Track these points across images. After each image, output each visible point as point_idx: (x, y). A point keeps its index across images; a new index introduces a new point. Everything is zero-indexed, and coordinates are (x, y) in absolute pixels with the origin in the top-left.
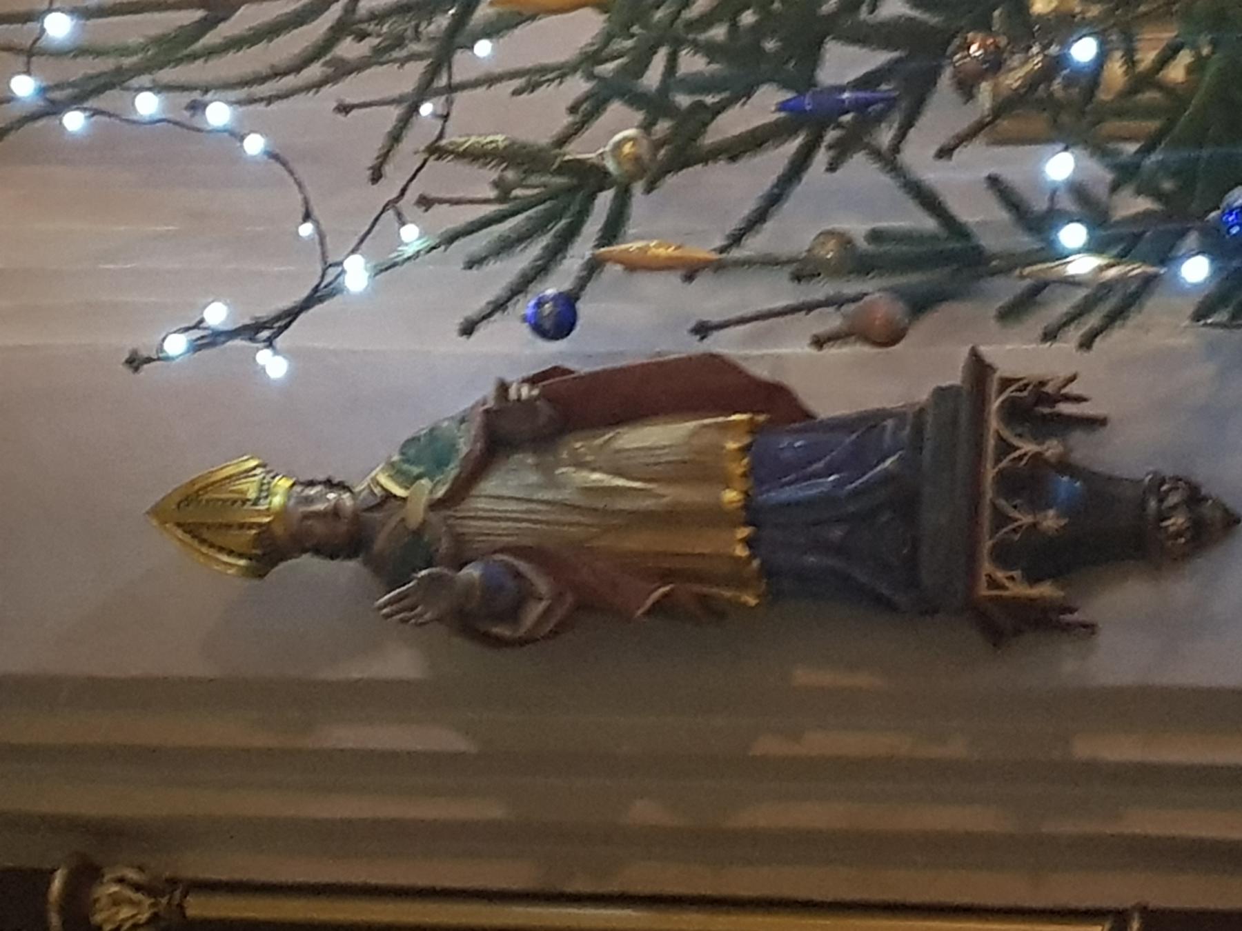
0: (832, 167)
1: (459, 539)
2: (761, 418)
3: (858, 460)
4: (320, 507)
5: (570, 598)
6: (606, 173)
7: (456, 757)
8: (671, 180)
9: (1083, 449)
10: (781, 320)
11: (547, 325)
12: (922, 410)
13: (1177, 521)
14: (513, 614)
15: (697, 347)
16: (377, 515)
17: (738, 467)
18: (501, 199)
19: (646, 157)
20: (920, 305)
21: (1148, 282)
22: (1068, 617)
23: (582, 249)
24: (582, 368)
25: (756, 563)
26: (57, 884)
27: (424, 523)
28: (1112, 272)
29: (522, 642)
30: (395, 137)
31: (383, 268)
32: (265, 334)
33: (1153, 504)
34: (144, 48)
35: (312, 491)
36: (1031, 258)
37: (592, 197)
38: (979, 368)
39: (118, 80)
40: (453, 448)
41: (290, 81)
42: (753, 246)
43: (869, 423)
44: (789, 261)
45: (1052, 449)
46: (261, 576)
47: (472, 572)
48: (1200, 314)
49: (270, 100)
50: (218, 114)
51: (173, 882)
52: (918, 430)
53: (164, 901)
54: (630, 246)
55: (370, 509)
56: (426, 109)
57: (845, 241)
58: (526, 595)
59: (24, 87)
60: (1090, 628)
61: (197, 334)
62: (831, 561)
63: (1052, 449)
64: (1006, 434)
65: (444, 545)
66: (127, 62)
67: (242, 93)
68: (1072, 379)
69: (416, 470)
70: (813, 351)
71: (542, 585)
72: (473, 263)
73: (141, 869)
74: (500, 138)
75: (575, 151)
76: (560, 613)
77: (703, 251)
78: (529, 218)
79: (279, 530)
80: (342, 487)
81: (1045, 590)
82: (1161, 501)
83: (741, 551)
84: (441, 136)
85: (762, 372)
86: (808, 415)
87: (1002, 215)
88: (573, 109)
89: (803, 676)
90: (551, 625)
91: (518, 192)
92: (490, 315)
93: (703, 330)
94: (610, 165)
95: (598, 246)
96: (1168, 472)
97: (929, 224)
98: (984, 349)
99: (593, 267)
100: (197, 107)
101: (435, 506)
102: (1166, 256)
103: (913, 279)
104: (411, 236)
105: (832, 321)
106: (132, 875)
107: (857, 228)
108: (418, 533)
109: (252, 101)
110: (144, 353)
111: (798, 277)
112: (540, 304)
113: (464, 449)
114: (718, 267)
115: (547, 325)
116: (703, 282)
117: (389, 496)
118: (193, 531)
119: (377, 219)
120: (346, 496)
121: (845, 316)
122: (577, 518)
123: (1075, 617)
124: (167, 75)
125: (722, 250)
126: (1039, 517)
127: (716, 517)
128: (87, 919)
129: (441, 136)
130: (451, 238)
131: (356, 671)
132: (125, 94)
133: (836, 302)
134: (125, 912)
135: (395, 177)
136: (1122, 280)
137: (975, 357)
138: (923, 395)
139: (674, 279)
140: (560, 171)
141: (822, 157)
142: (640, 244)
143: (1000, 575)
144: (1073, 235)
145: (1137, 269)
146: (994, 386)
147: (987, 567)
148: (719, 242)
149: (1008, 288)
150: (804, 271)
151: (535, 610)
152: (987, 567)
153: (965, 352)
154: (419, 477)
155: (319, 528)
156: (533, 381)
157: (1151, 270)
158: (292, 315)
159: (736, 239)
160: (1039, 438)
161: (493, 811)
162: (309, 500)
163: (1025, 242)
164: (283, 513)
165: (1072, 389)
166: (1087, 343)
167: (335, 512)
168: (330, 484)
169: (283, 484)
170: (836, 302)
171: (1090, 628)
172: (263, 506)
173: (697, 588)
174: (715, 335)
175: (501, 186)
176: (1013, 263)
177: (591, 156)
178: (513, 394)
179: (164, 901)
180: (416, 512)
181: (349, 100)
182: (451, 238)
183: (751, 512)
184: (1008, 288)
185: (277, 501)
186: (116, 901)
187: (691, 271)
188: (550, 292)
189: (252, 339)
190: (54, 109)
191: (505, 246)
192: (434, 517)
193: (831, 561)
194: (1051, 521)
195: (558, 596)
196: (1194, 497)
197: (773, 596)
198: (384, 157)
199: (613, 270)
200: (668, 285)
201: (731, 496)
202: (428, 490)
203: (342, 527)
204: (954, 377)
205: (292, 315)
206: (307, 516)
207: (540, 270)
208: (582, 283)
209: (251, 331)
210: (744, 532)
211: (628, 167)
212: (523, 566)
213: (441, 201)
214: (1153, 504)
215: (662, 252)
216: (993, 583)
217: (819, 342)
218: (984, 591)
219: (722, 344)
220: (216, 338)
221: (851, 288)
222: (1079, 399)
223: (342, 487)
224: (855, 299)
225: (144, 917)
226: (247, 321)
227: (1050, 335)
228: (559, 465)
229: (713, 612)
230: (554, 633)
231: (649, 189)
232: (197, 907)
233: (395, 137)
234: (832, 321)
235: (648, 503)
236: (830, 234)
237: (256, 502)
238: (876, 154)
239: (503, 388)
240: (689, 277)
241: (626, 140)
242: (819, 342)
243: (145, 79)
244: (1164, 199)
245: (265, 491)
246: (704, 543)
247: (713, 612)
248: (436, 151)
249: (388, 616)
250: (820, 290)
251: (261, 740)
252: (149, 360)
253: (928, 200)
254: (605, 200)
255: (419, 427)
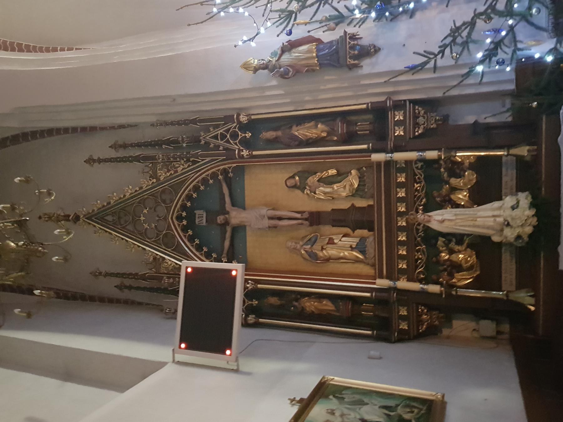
0: (323, 7)
1: (280, 65)
2: (317, 43)
3: (330, 47)
4: (262, 63)
5: (295, 72)
6: (294, 11)
7: (282, 94)
8: (302, 11)
9: (361, 42)
10: (319, 29)
11: (288, 34)
12: (338, 40)
13: (372, 50)
14: (288, 74)
15: (308, 34)
16: (269, 63)
17: (315, 50)
18: (280, 17)
19: (299, 8)
20: (337, 24)
21: (367, 17)
22: (359, 65)
23: (292, 23)
24: (293, 40)
25: (318, 63)
26: (237, 152)
27: (275, 64)
28: (363, 16)
29: (289, 78)
30: (265, 10)
31: (266, 29)
32: (251, 40)
33: (369, 48)
34: (229, 2)
35: (260, 61)
36: (351, 16)
37: (292, 14)
38: (345, 32)
39: (227, 7)
40: (278, 53)
41: (250, 4)
42: (314, 20)
43: (331, 42)
44: (319, 21)
45: (356, 42)
46: (255, 73)
47: (282, 69)
48: (374, 21)
49: (247, 7)
50: (241, 10)
51: (249, 114)
52: (338, 43)
53: (249, 117)
54: (298, 21)
55: (268, 63)
56: (269, 5)
57: (326, 17)
58: (289, 71)
59: (215, 10)
60: (362, 66)
61: (242, 41)
62: (328, 62)
63: (356, 42)
64: (349, 41)
65: (278, 66)
66: (228, 4)
67: (243, 7)
68: (358, 32)
69: (273, 56)
70: (323, 33)
71: (291, 70)
72: (277, 26)
73: (245, 113)
74: (279, 8)
75: (289, 9)
76: (294, 74)
77: (308, 21)
78: (284, 19)
79: (257, 67)
80: (264, 60)
81: (356, 62)
82: (370, 48)
83: (316, 62)
84: (271, 9)
85: (317, 37)
86: (323, 42)
87: (346, 10)
88: (287, 3)
89: (327, 78)
90: (293, 75)
91: (281, 16)
92: (280, 33)
93: (309, 32)
94: (294, 10)
95: (294, 22)
96: (371, 43)
97: (337, 13)
98: (346, 30)
99: (293, 25)
100: (238, 9)
101: (276, 61)
102: (370, 13)
103: (336, 21)
104: (269, 24)
105: (325, 28)
106: (244, 114)
107: (327, 15)
108: (274, 65)
109: (245, 8)
110: (237, 45)
111: (320, 23)
112: (287, 31)
113: (279, 53)
114: (309, 23)
115: (288, 34)
116: (308, 25)
117: (270, 60)
118: (246, 68)
119: (264, 22)
120: (265, 61)
121: (328, 28)
122: (294, 60)
123: (360, 65)
124: (234, 5)
125: (310, 20)
126: (355, 52)
127: (313, 58)
128: (239, 120)
129: (271, 9)
130: (274, 24)
131: (268, 84)
132: (228, 9)
133: (326, 25)
134: (244, 119)
135: (266, 15)
136: (364, 17)
137: (345, 31)
138: (338, 37)
139: (304, 25)
140: (288, 12)
141: (322, 5)
142: (299, 21)
143: (350, 60)
144: (357, 12)
145: (366, 15)
146: (347, 35)
147: (348, 60)
148: (309, 19)
149: (348, 21)
150: (321, 22)
151: (291, 73)
152: (348, 60)
153: (343, 31)
154: (273, 57)
155: (262, 66)
156: (287, 42)
157: (368, 15)
158: (255, 37)
159: (311, 19)
160: (354, 41)
161: (288, 100)
162: (260, 62)
163: (349, 14)
164: (257, 65)
165: (358, 34)
166: (359, 27)
167: (264, 63)
168: (262, 60)
169: (256, 61)
170: (326, 25)
171: (362, 66)
172: (254, 64)
173: (311, 68)
174: (311, 32)
175: (280, 15)
176: (348, 17)
177: (291, 9)
178: (285, 44)
179: (249, 117)
180: (274, 62)
181: (257, 6)
182: (274, 24)
183: (317, 56)
184: (348, 21)
185: (256, 63)
186: (243, 118)
187: (306, 24)
188: (288, 29)
189: (250, 41)
190: (219, 12)
191: (281, 24)
192: (276, 63)
193: (328, 62)
194: (356, 52)
195: (293, 71)
196: (375, 46)
197: (320, 68)
198: (264, 13)
199: (296, 25)
200: (303, 27)
201: (314, 55)
202: (275, 59)
203: (265, 65)
204: (342, 34)
205: (255, 37)
206: (260, 65)
207: (287, 26)
208: (292, 27)
209: (249, 40)
210: (317, 59)
211: (297, 10)
212: (289, 68)
213: (271, 19)
214: (369, 48)
215: (302, 21)
216: (349, 62)
217: (324, 32)
218: (348, 63)
219: (312, 34)
220: (245, 41)
221: (328, 23)
222: (359, 35)
223: (264, 60)
224: (329, 25)
225: (246, 119)
226: (249, 39)
227: (355, 26)
228: (291, 53)
229: (314, 71)
230: (293, 76)
231: (299, 13)
232: (253, 117)
233: (265, 10)
234: (325, 28)
235: (303, 57)
236: (324, 16)
237: (253, 64)
238: (329, 4)
239: (283, 44)
240: (306, 25)
241: (296, 6)
242: (324, 32)
243: (230, 6)
244: (126, 126)
245: (254, 62)
246: (311, 62)
247: (314, 71)
248: (271, 11)
249: (272, 76)
250: (324, 24)
251: (257, 95)
252: (237, 46)
253: (336, 10)
254: (294, 15)
255: (272, 51)
